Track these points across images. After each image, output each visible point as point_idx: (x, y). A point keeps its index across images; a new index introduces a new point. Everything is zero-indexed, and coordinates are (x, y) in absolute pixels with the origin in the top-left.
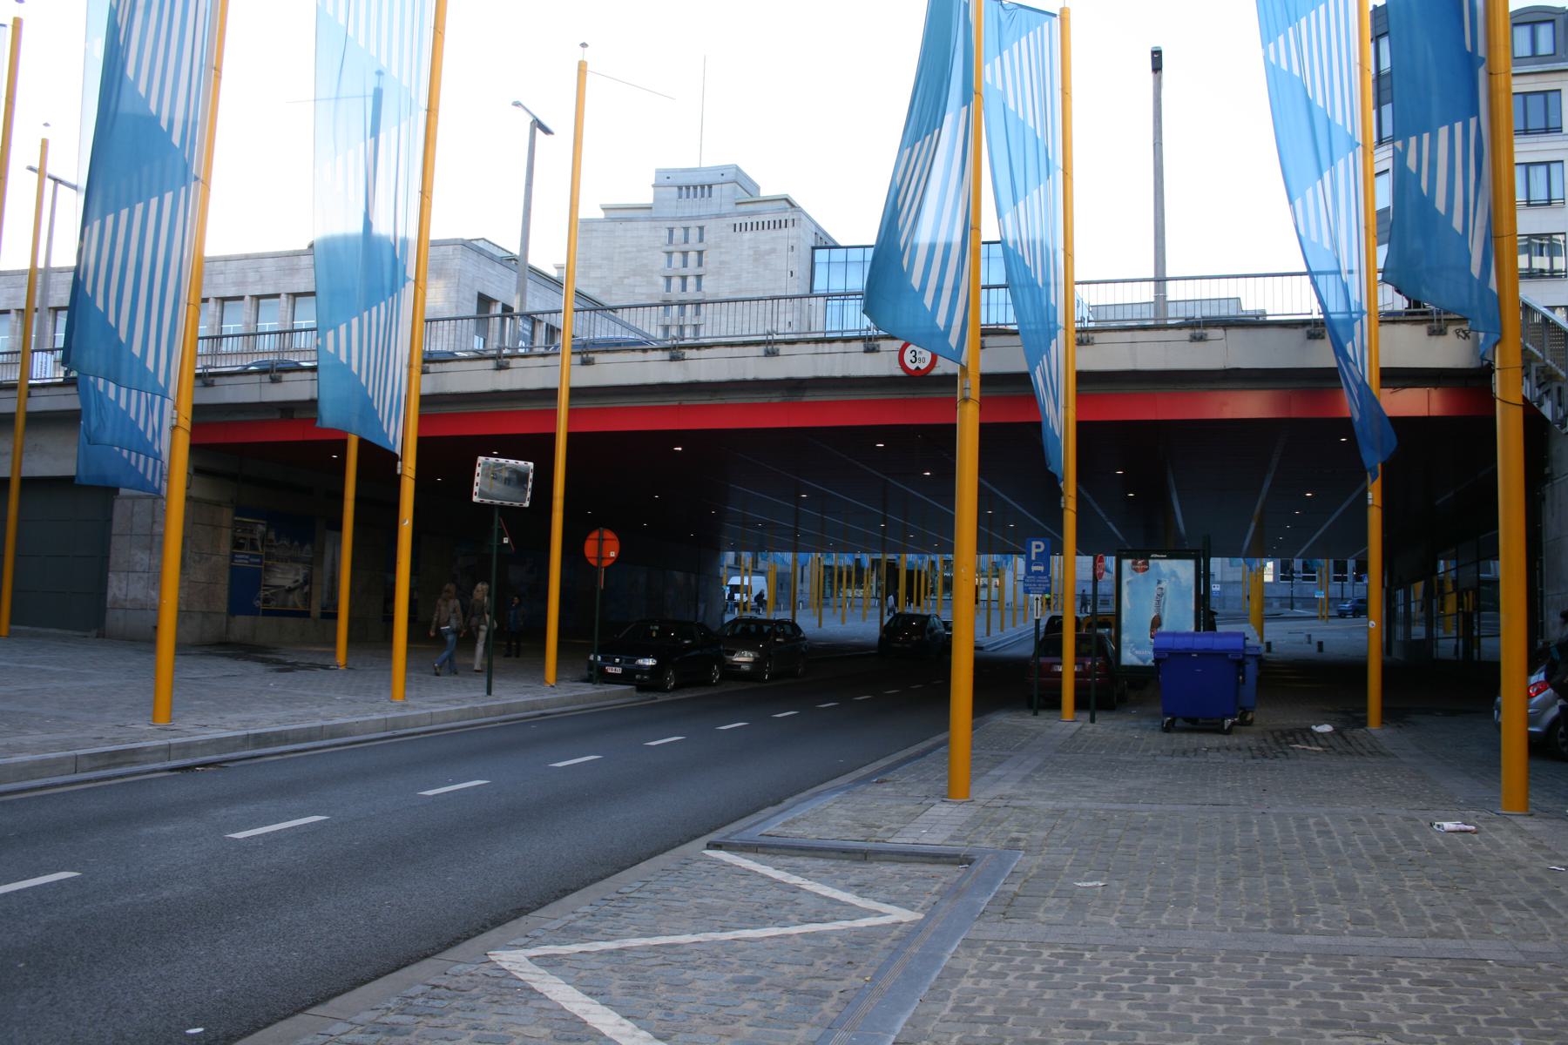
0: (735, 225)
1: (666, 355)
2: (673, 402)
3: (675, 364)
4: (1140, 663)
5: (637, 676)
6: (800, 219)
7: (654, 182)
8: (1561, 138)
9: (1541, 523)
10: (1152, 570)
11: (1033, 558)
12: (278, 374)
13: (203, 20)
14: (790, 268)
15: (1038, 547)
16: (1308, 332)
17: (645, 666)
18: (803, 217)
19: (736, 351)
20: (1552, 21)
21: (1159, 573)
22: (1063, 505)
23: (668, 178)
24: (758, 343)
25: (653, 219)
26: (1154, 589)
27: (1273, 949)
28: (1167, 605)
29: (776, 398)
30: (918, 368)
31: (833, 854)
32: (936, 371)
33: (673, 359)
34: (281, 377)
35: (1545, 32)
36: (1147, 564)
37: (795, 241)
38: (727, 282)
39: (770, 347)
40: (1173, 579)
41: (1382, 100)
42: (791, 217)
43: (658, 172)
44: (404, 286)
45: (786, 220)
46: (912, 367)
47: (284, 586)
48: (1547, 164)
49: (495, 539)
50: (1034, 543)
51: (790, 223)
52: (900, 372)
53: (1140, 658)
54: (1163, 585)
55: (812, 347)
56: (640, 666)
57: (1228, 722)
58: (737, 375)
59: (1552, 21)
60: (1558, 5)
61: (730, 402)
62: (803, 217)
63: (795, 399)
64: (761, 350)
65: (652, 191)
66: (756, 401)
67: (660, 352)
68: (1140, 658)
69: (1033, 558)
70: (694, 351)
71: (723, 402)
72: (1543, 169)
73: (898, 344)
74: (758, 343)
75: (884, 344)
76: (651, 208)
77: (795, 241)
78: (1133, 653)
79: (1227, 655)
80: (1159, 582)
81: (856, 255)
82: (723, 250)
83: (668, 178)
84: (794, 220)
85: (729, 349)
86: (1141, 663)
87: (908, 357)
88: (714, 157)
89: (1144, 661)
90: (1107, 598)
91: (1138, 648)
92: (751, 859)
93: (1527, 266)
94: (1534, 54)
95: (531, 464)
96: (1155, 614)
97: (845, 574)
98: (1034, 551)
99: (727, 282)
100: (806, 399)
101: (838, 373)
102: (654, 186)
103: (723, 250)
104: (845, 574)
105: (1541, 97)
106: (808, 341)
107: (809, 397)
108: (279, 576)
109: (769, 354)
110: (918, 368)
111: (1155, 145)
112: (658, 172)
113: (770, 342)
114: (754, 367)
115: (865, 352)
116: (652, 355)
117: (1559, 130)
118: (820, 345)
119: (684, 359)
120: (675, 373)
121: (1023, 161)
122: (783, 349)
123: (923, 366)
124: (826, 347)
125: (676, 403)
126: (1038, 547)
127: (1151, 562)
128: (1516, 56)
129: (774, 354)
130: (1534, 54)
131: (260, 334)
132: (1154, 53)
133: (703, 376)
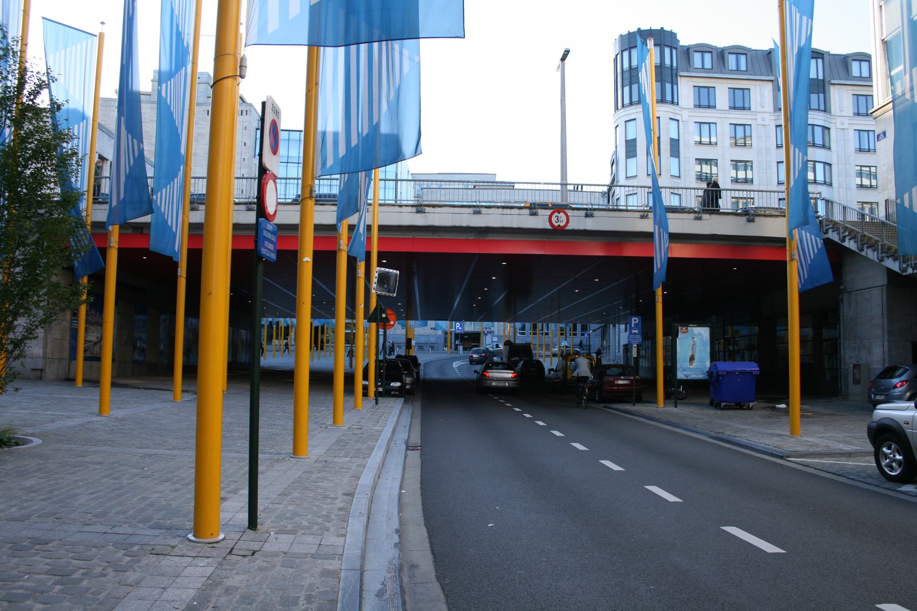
0: (208, 111)
1: (414, 209)
2: (409, 236)
4: (685, 378)
5: (392, 393)
6: (251, 111)
7: (152, 78)
10: (689, 333)
11: (633, 326)
13: (740, 82)
14: (244, 141)
15: (635, 320)
17: (396, 387)
18: (253, 109)
20: (711, 52)
22: (179, 274)
24: (469, 207)
26: (690, 342)
28: (697, 349)
30: (559, 225)
32: (569, 227)
33: (418, 212)
36: (687, 329)
37: (247, 124)
38: (202, 147)
39: (477, 209)
41: (633, 81)
42: (245, 109)
44: (510, 186)
45: (242, 111)
47: (92, 341)
48: (709, 123)
49: (379, 315)
50: (633, 319)
51: (244, 113)
52: (548, 226)
53: (685, 376)
54: (695, 340)
55: (500, 210)
56: (393, 387)
57: (723, 404)
58: (457, 223)
59: (711, 52)
60: (714, 44)
62: (253, 109)
63: (482, 238)
64: (471, 210)
65: (151, 84)
67: (410, 208)
68: (685, 376)
69: (633, 326)
70: (431, 208)
72: (707, 126)
73: (549, 212)
74: (469, 207)
75: (540, 212)
76: (150, 95)
77: (247, 124)
80: (693, 338)
84: (247, 111)
85: (452, 208)
87: (554, 219)
88: (249, 72)
89: (687, 377)
91: (684, 371)
93: (744, 177)
94: (703, 68)
95: (398, 272)
98: (633, 322)
99: (202, 147)
100: (488, 238)
101: (515, 225)
103: (200, 126)
104: (320, 330)
105: (706, 89)
106: (498, 207)
108: (91, 334)
109: (476, 213)
110: (559, 225)
111: (561, 100)
114: (467, 219)
115: (530, 215)
117: (715, 107)
118: (505, 210)
120: (419, 220)
121: (680, 131)
122: (484, 210)
124: (509, 211)
125: (412, 237)
126: (635, 320)
127: (689, 328)
129: (479, 213)
130: (703, 68)
132: (566, 51)
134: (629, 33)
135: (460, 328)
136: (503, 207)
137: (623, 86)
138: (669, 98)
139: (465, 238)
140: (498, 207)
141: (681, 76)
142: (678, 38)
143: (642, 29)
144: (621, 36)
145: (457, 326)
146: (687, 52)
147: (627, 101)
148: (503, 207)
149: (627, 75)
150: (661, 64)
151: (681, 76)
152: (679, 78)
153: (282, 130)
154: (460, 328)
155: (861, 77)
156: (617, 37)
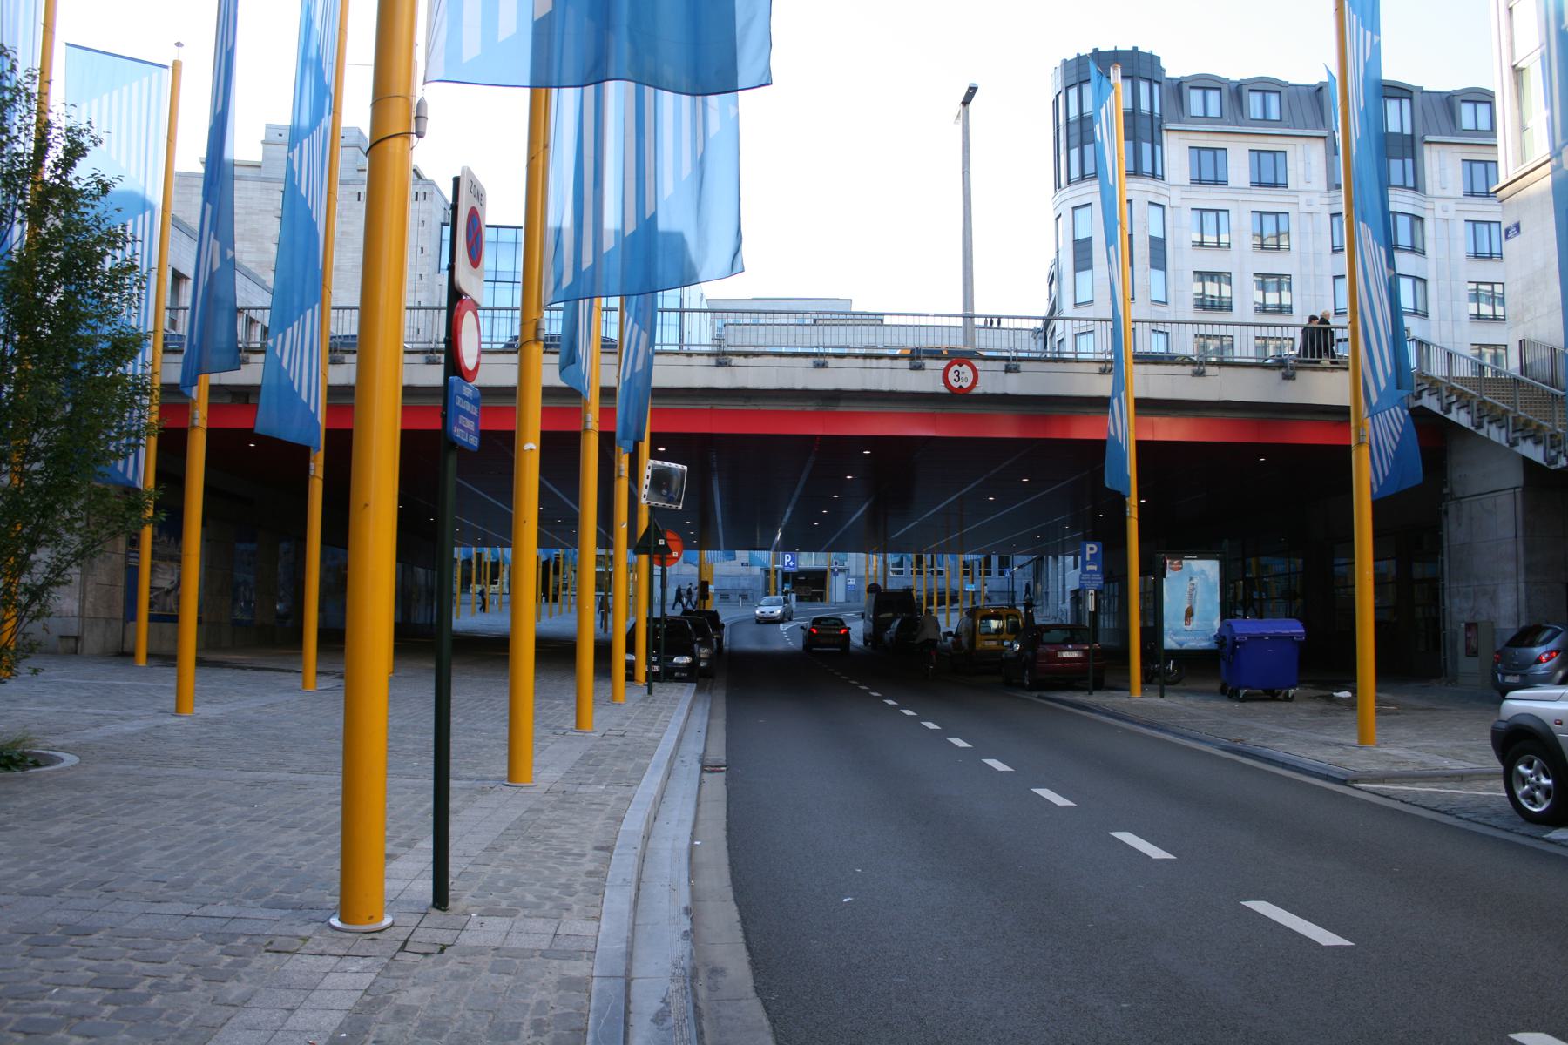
0: (359, 193)
1: (712, 361)
3: (721, 370)
6: (432, 193)
8: (1226, 190)
9: (399, 509)
11: (1088, 558)
12: (245, 355)
14: (420, 245)
15: (1092, 549)
16: (1283, 374)
18: (435, 191)
19: (784, 361)
21: (1191, 572)
23: (280, 135)
25: (265, 180)
26: (1187, 586)
27: (348, 976)
29: (810, 407)
30: (961, 387)
31: (1439, 779)
32: (978, 390)
33: (719, 365)
34: (248, 358)
35: (1213, 97)
39: (820, 360)
40: (1203, 576)
42: (423, 190)
43: (269, 127)
46: (956, 385)
50: (1088, 546)
51: (421, 197)
52: (943, 390)
54: (1195, 581)
55: (860, 361)
58: (786, 383)
59: (1220, 89)
61: (763, 408)
62: (435, 191)
64: (809, 361)
65: (260, 148)
66: (790, 408)
67: (705, 358)
69: (1088, 558)
70: (742, 358)
71: (756, 408)
72: (1213, 215)
73: (943, 364)
75: (929, 363)
76: (260, 167)
78: (1172, 639)
79: (1263, 638)
80: (1191, 579)
81: (508, 235)
82: (345, 219)
83: (280, 135)
85: (778, 358)
86: (1178, 647)
87: (952, 376)
88: (431, 127)
89: (1181, 645)
90: (746, 593)
91: (1175, 634)
92: (1476, 780)
94: (1206, 116)
95: (686, 468)
96: (1188, 606)
97: (552, 565)
98: (1088, 552)
100: (840, 409)
101: (885, 387)
102: (263, 142)
103: (345, 219)
104: (552, 565)
105: (1212, 153)
106: (857, 356)
107: (842, 408)
109: (817, 366)
110: (961, 387)
112: (269, 127)
113: (822, 355)
114: (803, 377)
115: (911, 369)
116: (695, 360)
117: (1226, 183)
118: (868, 360)
119: (730, 366)
120: (721, 379)
121: (1168, 224)
122: (832, 362)
123: (965, 385)
124: (874, 363)
125: (708, 407)
126: (1092, 549)
127: (1184, 562)
128: (1219, 115)
130: (1206, 116)
131: (181, 308)
132: (970, 88)
133: (752, 383)
134: (1079, 57)
135: (791, 564)
136: (865, 356)
137: (1068, 149)
138: (1147, 167)
139: (800, 409)
140: (857, 356)
141: (1168, 130)
142: (1163, 64)
143: (1100, 50)
144: (1065, 62)
145: (786, 561)
146: (1178, 89)
147: (1075, 173)
148: (865, 356)
149: (1075, 129)
150: (1133, 109)
151: (1168, 130)
152: (1164, 133)
153: (488, 226)
154: (791, 564)
155: (1476, 130)
156: (1058, 64)
